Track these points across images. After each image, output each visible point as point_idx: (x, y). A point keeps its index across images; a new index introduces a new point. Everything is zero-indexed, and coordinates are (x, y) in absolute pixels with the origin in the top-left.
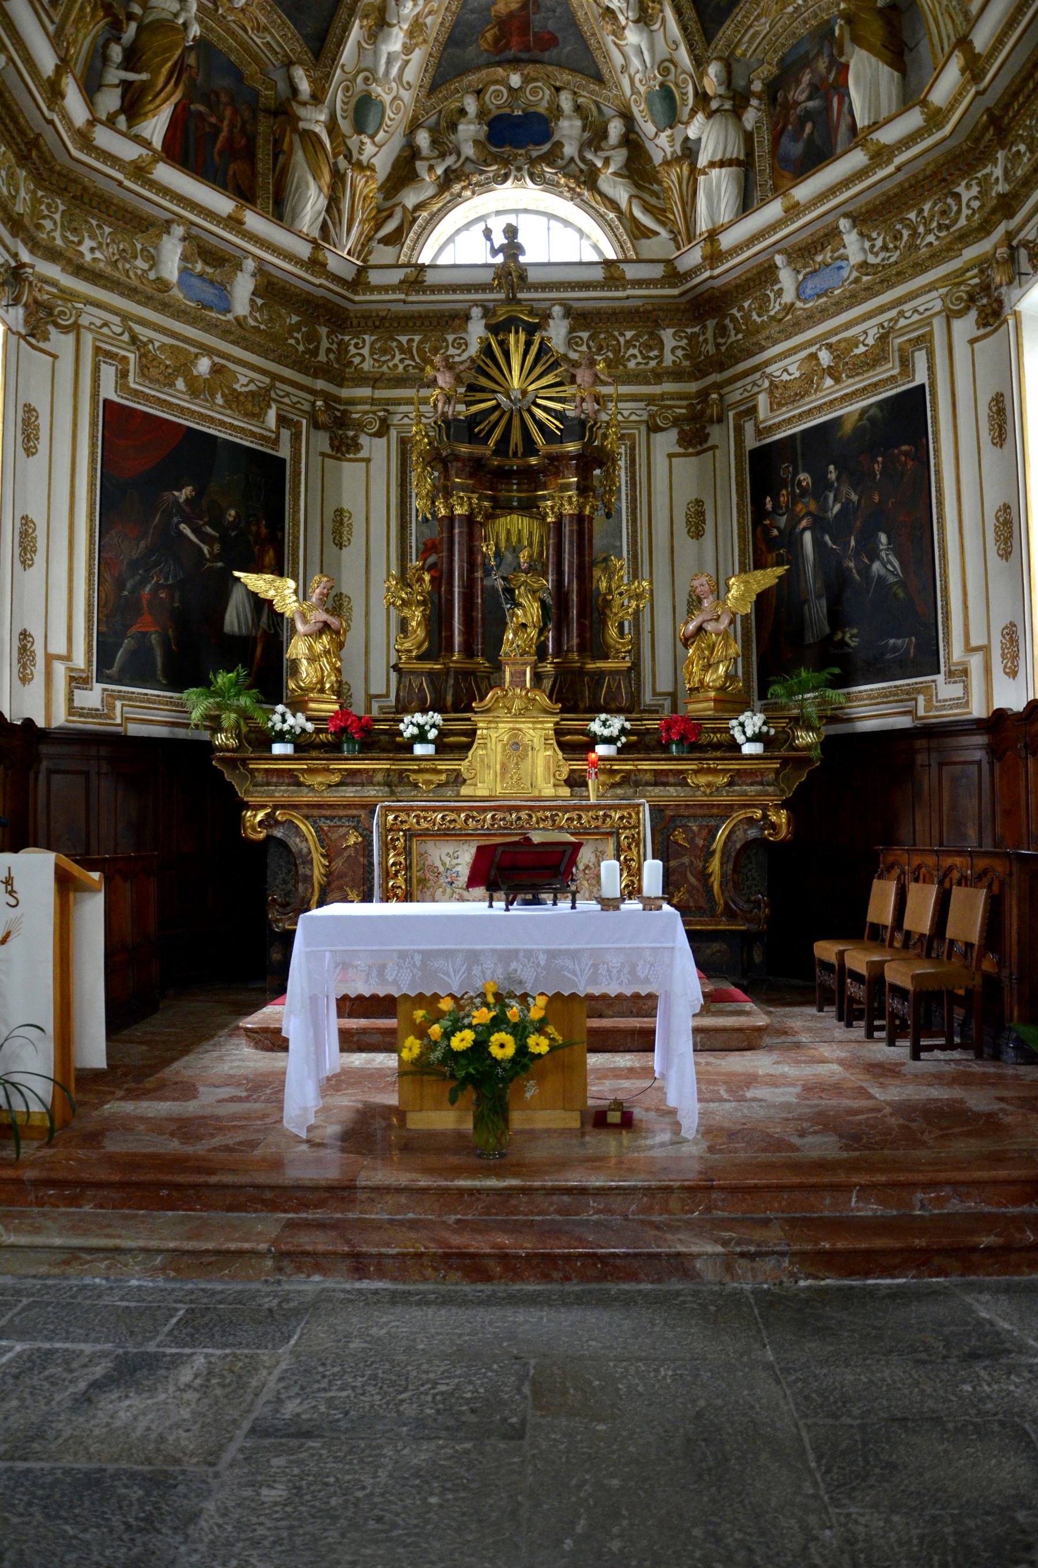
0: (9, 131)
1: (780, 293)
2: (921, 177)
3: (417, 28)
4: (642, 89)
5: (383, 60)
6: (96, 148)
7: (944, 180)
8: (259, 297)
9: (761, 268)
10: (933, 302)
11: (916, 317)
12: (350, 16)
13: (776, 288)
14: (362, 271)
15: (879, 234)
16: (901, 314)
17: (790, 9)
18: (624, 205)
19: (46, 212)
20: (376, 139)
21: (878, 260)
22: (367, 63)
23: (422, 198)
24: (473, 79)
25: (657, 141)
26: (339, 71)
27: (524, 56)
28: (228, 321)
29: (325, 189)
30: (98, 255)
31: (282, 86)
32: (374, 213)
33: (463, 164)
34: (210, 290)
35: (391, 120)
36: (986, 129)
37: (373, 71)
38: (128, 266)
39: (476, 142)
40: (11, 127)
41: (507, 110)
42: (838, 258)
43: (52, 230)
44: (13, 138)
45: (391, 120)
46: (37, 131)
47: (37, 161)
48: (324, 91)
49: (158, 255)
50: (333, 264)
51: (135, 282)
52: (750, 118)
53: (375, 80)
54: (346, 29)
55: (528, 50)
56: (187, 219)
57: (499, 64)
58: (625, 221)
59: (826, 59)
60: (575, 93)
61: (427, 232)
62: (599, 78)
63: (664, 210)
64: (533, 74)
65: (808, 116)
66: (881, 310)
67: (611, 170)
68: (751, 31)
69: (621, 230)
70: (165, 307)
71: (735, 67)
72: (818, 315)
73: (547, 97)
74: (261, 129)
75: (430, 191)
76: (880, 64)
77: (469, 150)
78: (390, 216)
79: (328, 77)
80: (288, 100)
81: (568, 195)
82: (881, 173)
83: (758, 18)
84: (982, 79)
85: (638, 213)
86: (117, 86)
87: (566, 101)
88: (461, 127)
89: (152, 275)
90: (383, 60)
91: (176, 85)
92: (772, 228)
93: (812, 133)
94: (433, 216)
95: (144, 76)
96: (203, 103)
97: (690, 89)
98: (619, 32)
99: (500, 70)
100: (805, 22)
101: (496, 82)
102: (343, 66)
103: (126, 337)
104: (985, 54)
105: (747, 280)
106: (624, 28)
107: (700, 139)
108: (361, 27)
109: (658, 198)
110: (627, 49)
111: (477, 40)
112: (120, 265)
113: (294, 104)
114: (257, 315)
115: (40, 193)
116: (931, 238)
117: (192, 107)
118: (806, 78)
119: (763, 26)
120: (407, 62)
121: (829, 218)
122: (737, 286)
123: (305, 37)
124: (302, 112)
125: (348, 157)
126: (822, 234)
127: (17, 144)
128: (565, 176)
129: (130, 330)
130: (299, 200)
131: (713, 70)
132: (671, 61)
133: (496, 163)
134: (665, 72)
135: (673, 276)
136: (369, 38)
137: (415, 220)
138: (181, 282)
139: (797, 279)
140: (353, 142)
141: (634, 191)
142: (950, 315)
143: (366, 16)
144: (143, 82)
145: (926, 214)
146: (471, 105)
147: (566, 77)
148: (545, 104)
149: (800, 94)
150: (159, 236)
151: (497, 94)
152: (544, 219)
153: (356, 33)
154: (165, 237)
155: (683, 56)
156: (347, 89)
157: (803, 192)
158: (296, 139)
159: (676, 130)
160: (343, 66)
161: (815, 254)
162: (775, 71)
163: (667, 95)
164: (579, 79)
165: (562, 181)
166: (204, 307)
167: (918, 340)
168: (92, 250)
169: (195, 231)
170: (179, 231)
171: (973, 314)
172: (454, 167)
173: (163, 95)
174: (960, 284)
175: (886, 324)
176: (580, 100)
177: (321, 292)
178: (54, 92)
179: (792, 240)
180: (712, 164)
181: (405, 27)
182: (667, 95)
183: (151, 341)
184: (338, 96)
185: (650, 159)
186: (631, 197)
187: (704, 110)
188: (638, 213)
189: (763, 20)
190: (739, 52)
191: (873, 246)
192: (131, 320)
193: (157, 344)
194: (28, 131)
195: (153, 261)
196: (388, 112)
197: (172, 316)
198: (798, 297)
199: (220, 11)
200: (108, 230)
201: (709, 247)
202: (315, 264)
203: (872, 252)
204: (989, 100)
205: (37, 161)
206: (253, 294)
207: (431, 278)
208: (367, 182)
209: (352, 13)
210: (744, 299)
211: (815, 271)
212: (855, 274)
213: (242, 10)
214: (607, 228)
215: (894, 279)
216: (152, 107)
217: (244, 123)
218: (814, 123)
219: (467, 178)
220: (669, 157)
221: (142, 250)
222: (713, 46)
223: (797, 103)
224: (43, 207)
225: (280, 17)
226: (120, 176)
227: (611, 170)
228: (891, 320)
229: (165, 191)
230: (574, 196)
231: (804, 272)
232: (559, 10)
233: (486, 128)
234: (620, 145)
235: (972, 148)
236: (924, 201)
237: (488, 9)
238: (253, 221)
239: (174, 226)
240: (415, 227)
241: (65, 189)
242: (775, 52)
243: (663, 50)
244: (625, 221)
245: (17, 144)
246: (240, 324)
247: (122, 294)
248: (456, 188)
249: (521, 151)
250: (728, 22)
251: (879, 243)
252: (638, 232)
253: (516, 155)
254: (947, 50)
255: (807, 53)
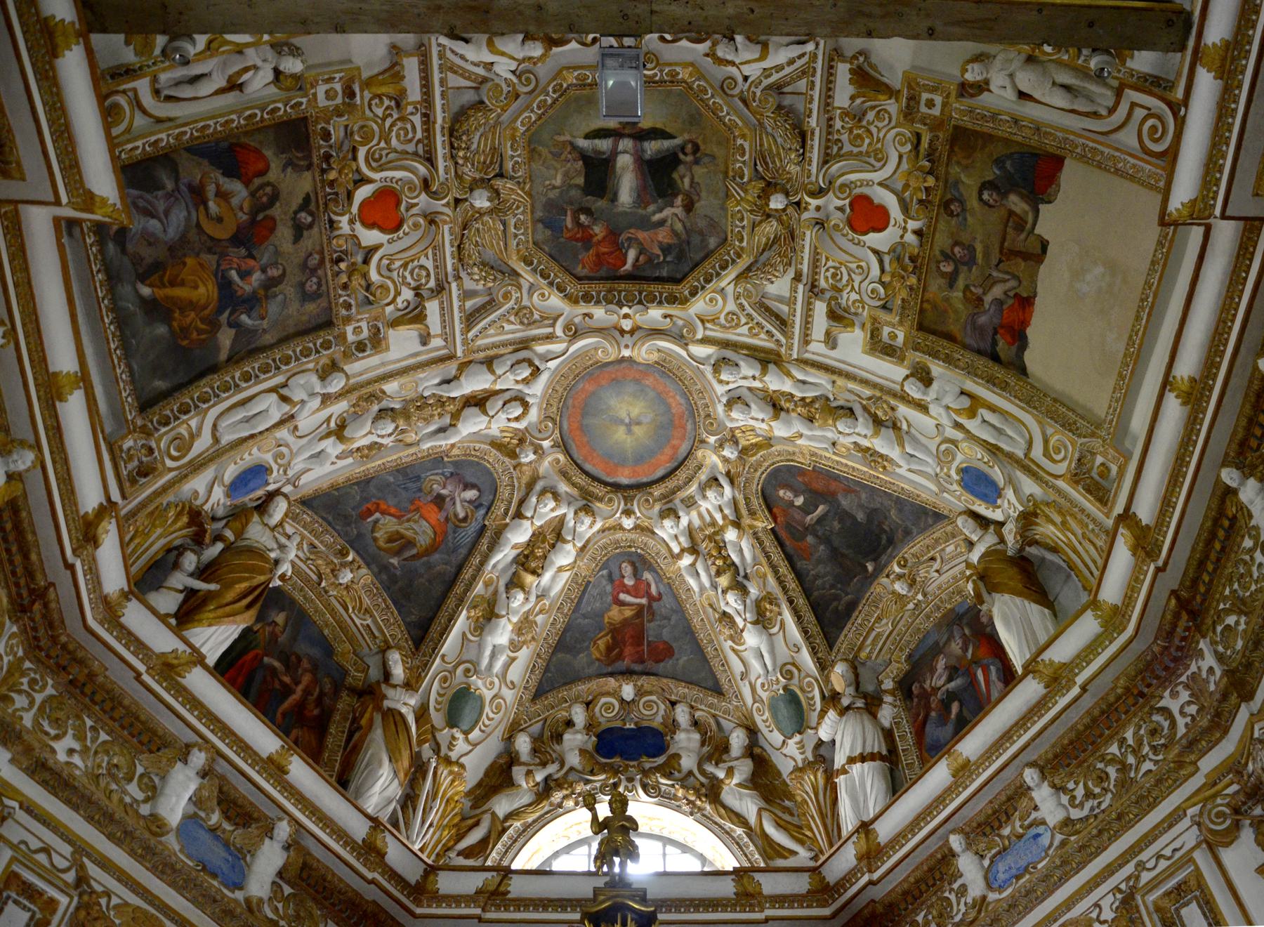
0: (11, 562)
1: (963, 890)
2: (1112, 699)
3: (525, 625)
4: (764, 695)
5: (488, 653)
6: (122, 627)
7: (1142, 694)
8: (288, 883)
9: (932, 862)
10: (1186, 836)
11: (1163, 864)
12: (457, 606)
13: (955, 886)
14: (431, 870)
15: (1077, 783)
16: (1141, 866)
17: (911, 606)
18: (753, 820)
19: (25, 687)
20: (470, 736)
21: (1086, 812)
22: (470, 655)
23: (516, 806)
24: (582, 688)
25: (784, 751)
26: (438, 660)
27: (638, 667)
28: (236, 901)
29: (402, 775)
30: (76, 760)
31: (375, 674)
32: (457, 820)
33: (567, 774)
34: (222, 852)
35: (489, 719)
36: (1177, 616)
37: (475, 664)
38: (114, 787)
39: (582, 752)
40: (18, 559)
41: (618, 724)
42: (1030, 826)
43: (23, 709)
44: (14, 573)
45: (489, 719)
46: (51, 579)
47: (38, 617)
48: (419, 679)
49: (163, 788)
50: (394, 854)
51: (113, 806)
52: (886, 714)
53: (476, 672)
54: (452, 619)
55: (642, 662)
56: (214, 746)
57: (611, 674)
58: (755, 838)
59: (960, 641)
60: (692, 707)
61: (518, 845)
62: (718, 691)
63: (800, 827)
64: (647, 687)
65: (952, 696)
66: (1110, 870)
67: (735, 780)
68: (873, 634)
69: (752, 848)
70: (149, 854)
71: (861, 670)
72: (1024, 901)
73: (662, 712)
74: (340, 706)
75: (526, 799)
76: (1026, 602)
77: (574, 760)
78: (477, 824)
79: (426, 666)
80: (378, 683)
81: (686, 808)
82: (1063, 702)
83: (879, 619)
84: (1159, 556)
85: (770, 829)
86: (181, 592)
87: (682, 715)
88: (566, 737)
89: (145, 810)
90: (488, 653)
91: (249, 607)
92: (940, 801)
93: (961, 710)
94: (527, 827)
95: (213, 587)
96: (279, 660)
97: (817, 693)
98: (737, 637)
99: (612, 680)
100: (928, 617)
101: (608, 694)
102: (443, 656)
103: (70, 877)
104: (1152, 524)
105: (917, 882)
106: (742, 631)
107: (833, 742)
108: (468, 618)
109: (792, 814)
110: (745, 654)
111: (588, 648)
112: (103, 782)
113: (383, 686)
114: (280, 906)
115: (27, 664)
116: (1147, 766)
117: (266, 659)
118: (941, 663)
119: (885, 627)
120: (513, 659)
121: (1009, 774)
122: (905, 893)
123: (408, 625)
124: (390, 692)
125: (437, 749)
126: (1004, 798)
127: (17, 585)
128: (682, 787)
129: (82, 867)
130: (365, 779)
131: (839, 669)
132: (794, 664)
133: (604, 771)
134: (788, 675)
135: (823, 891)
136: (475, 630)
137: (504, 830)
138: (181, 830)
139: (982, 866)
140: (444, 735)
141: (763, 804)
142: (1214, 843)
143: (475, 607)
144: (209, 592)
145: (1130, 742)
146: (579, 715)
147: (682, 690)
148: (659, 719)
149: (938, 679)
150: (171, 762)
151: (608, 707)
152: (659, 845)
153: (461, 623)
154: (179, 765)
155: (806, 658)
156: (445, 679)
157: (972, 745)
158: (378, 718)
159: (805, 736)
160: (443, 656)
161: (1000, 827)
162: (906, 667)
163: (792, 699)
164: (694, 692)
165: (680, 793)
166: (204, 869)
167: (1180, 892)
168: (71, 752)
169: (221, 766)
170: (199, 759)
171: (1247, 835)
172: (556, 777)
173: (228, 609)
174: (1214, 796)
175: (1123, 886)
176: (698, 714)
177: (370, 893)
178: (88, 535)
179: (968, 812)
180: (851, 760)
181: (515, 619)
182: (792, 699)
183: (108, 894)
184: (433, 685)
185: (779, 774)
186: (760, 810)
187: (834, 706)
188: (770, 829)
189: (884, 621)
190: (863, 655)
191: (1073, 798)
192: (89, 856)
193: (115, 901)
194: (39, 576)
195: (153, 793)
196: (487, 709)
197: (153, 870)
198: (989, 886)
199: (323, 584)
200: (103, 737)
201: (863, 841)
202: (370, 851)
203: (1074, 806)
204: (1172, 579)
205: (38, 617)
206: (280, 874)
207: (517, 888)
208: (453, 781)
209: (461, 601)
210: (916, 912)
211: (1005, 849)
212: (1059, 838)
213: (347, 588)
214: (735, 847)
215: (1116, 826)
216: (211, 615)
217: (322, 694)
218: (960, 701)
219: (571, 785)
220: (800, 765)
221: (142, 776)
222: (835, 649)
223: (935, 690)
224: (25, 680)
225: (384, 600)
226: (142, 668)
227: (735, 780)
228: (1128, 879)
229: (194, 703)
230: (694, 811)
231: (989, 855)
232: (674, 618)
233: (594, 739)
234: (743, 756)
235: (1166, 648)
236: (1124, 727)
237: (603, 616)
238: (300, 772)
239: (195, 751)
240: (505, 838)
241: (64, 668)
242: (901, 650)
243: (784, 653)
244: (755, 838)
245: (17, 585)
246: (250, 910)
247: (90, 819)
248: (557, 796)
249: (632, 763)
250: (849, 625)
251: (1080, 792)
252: (770, 849)
253: (627, 766)
254: (1096, 573)
255: (937, 643)
